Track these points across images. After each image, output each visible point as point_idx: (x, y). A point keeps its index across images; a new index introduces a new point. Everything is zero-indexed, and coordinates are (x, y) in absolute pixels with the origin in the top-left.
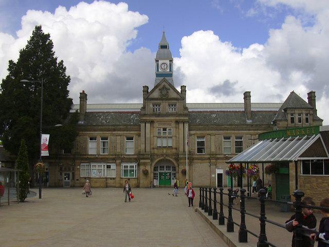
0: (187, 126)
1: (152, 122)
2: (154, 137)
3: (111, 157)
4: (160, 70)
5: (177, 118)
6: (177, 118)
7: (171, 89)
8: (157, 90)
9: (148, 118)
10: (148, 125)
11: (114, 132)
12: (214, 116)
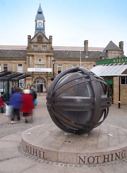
7: (44, 37)
10: (31, 58)
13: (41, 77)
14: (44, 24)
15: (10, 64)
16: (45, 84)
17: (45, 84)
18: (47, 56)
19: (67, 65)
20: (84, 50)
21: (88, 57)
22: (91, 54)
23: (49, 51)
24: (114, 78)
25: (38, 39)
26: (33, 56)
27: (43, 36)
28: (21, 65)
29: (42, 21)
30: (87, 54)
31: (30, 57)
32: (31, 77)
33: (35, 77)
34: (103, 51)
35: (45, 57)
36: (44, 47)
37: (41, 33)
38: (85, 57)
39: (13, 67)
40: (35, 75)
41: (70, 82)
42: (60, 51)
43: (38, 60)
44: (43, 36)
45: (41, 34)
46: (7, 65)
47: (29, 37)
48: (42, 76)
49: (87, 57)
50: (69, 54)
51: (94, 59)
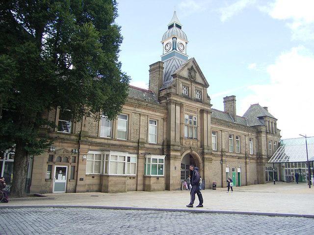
1: (181, 105)
3: (131, 144)
5: (203, 107)
6: (203, 107)
8: (186, 68)
9: (178, 100)
10: (178, 108)
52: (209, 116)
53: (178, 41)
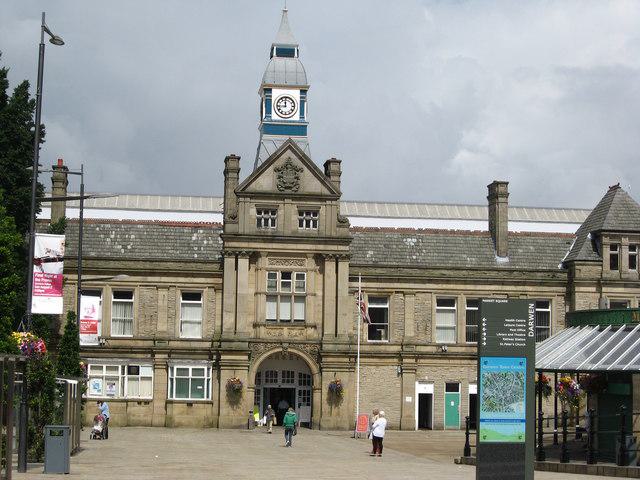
0: (344, 267)
2: (256, 294)
4: (274, 116)
7: (305, 169)
10: (243, 263)
11: (150, 279)
12: (411, 241)
13: (291, 354)
14: (302, 103)
15: (145, 291)
16: (302, 388)
17: (302, 388)
18: (320, 259)
19: (413, 298)
20: (219, 219)
21: (506, 260)
22: (519, 245)
23: (328, 234)
24: (627, 386)
25: (279, 177)
26: (254, 257)
27: (299, 164)
28: (197, 296)
29: (295, 94)
30: (502, 245)
31: (340, 264)
32: (246, 354)
33: (261, 354)
34: (578, 226)
35: (310, 263)
36: (308, 213)
37: (290, 146)
38: (491, 259)
39: (160, 303)
40: (261, 347)
41: (399, 390)
42: (376, 230)
43: (279, 275)
44: (299, 164)
45: (293, 156)
46: (545, 304)
47: (231, 164)
48: (295, 351)
49: (502, 261)
50: (416, 249)
51: (538, 271)
52: (344, 267)
53: (276, 94)
